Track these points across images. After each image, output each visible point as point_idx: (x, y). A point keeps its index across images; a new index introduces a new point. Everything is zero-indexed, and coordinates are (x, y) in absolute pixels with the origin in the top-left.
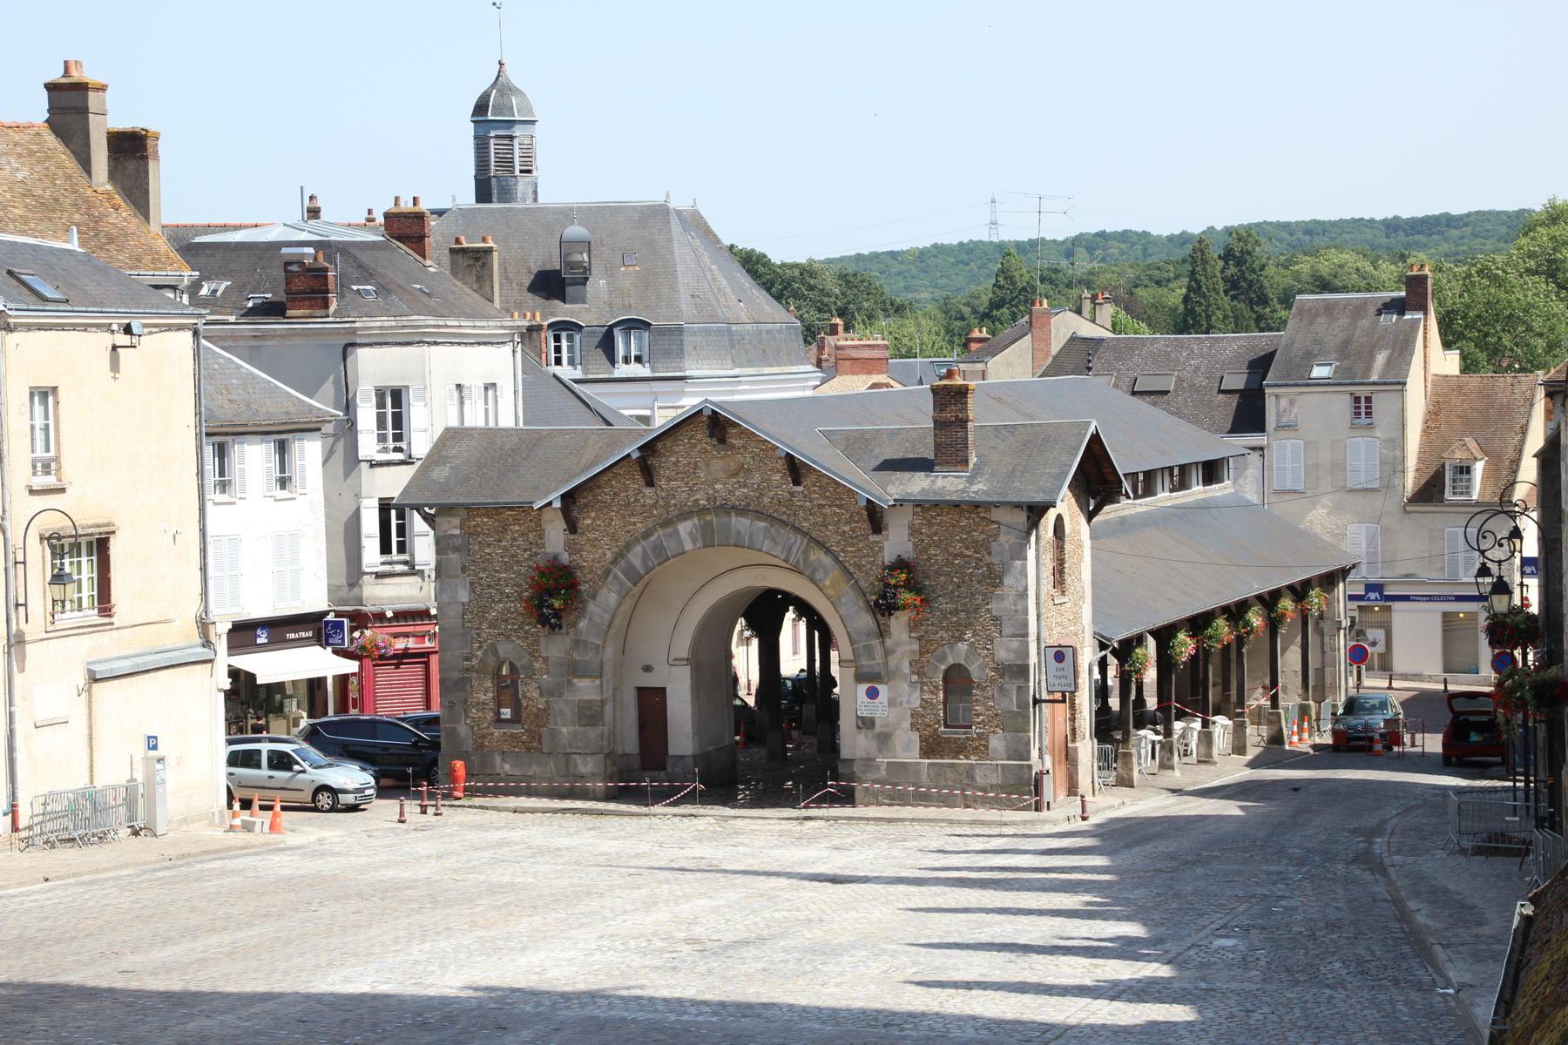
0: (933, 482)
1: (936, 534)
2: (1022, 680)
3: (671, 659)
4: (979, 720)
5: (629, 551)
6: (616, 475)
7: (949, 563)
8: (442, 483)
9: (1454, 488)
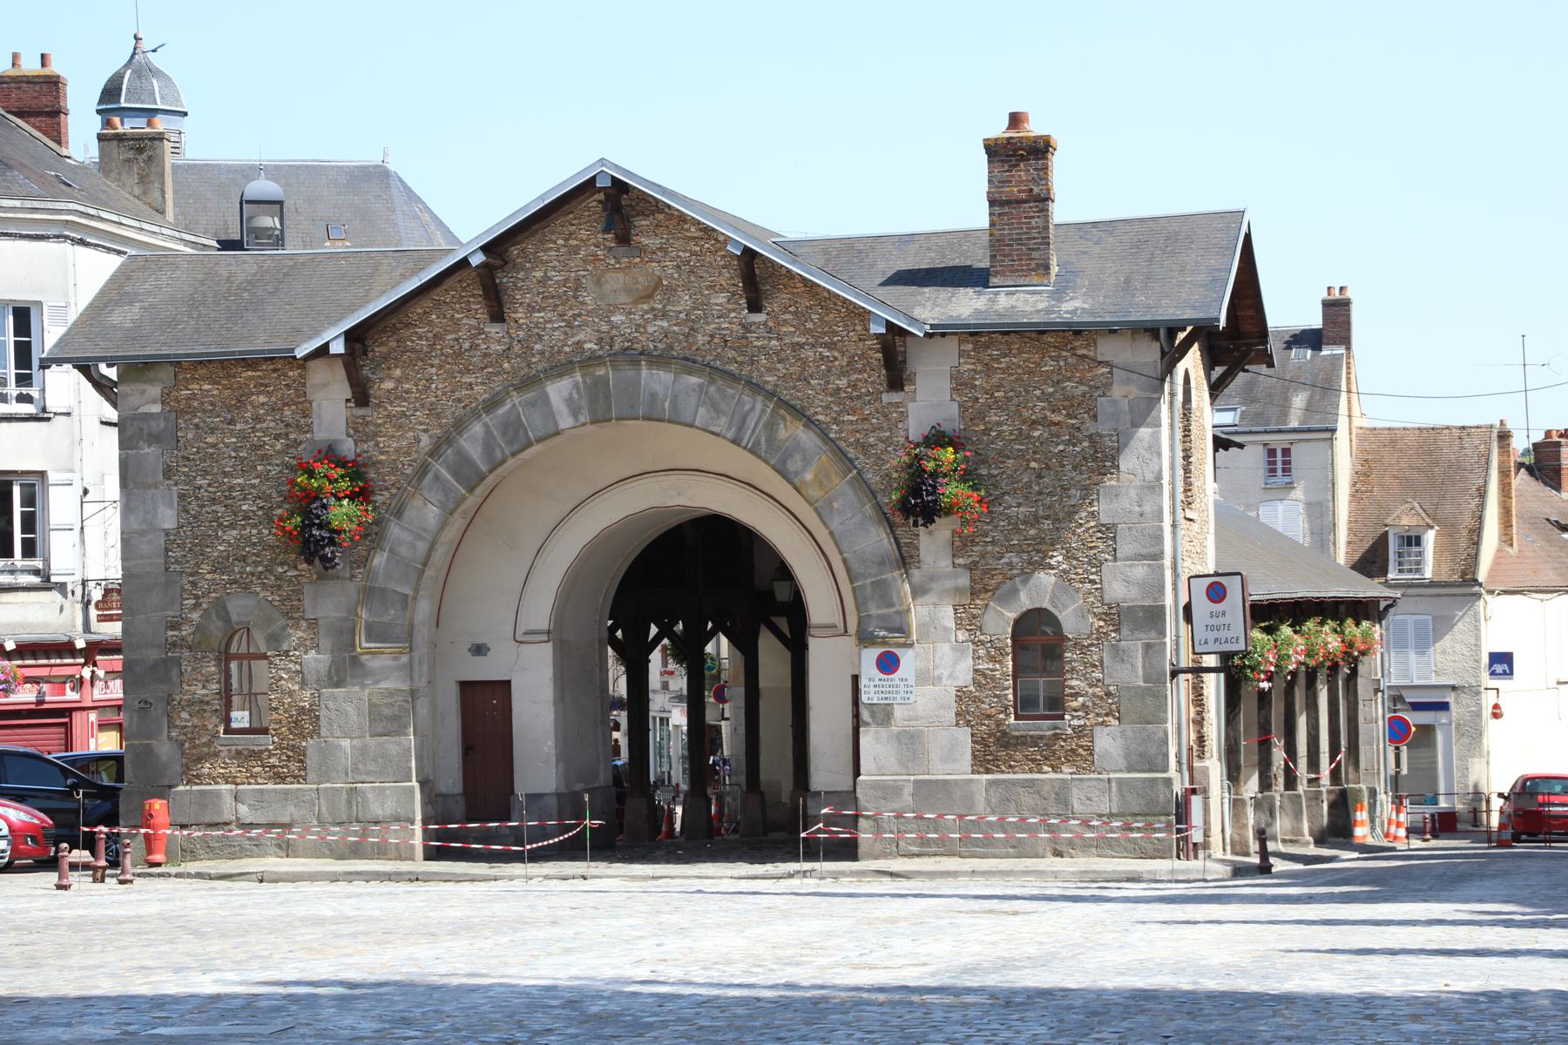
0: (993, 301)
1: (998, 387)
2: (1153, 634)
3: (520, 631)
4: (1074, 704)
5: (460, 434)
6: (438, 305)
7: (1021, 437)
8: (128, 330)
9: (1400, 564)
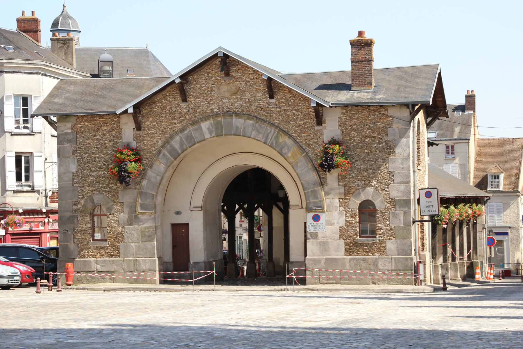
1: (354, 124)
2: (407, 209)
3: (192, 206)
4: (380, 232)
5: (172, 140)
6: (164, 96)
7: (362, 141)
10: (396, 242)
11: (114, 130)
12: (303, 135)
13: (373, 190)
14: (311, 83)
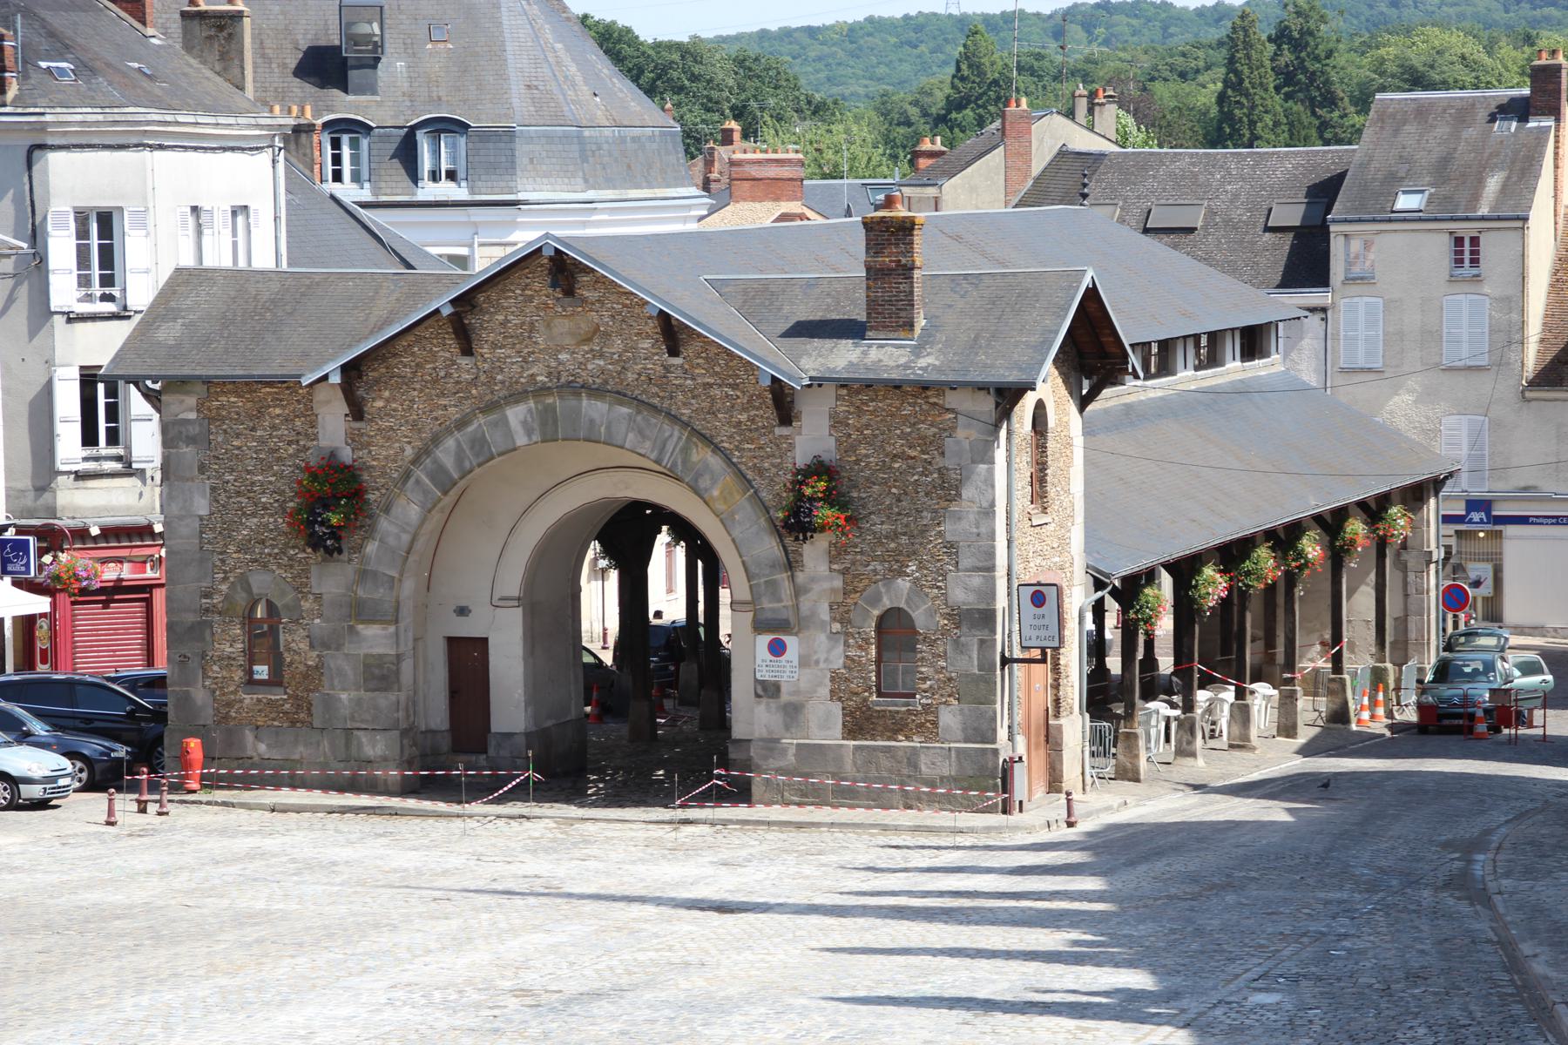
1: (867, 426)
2: (986, 632)
3: (496, 597)
4: (925, 686)
5: (437, 446)
6: (419, 339)
7: (885, 467)
10: (961, 710)
11: (297, 416)
12: (746, 446)
13: (908, 585)
14: (780, 309)
